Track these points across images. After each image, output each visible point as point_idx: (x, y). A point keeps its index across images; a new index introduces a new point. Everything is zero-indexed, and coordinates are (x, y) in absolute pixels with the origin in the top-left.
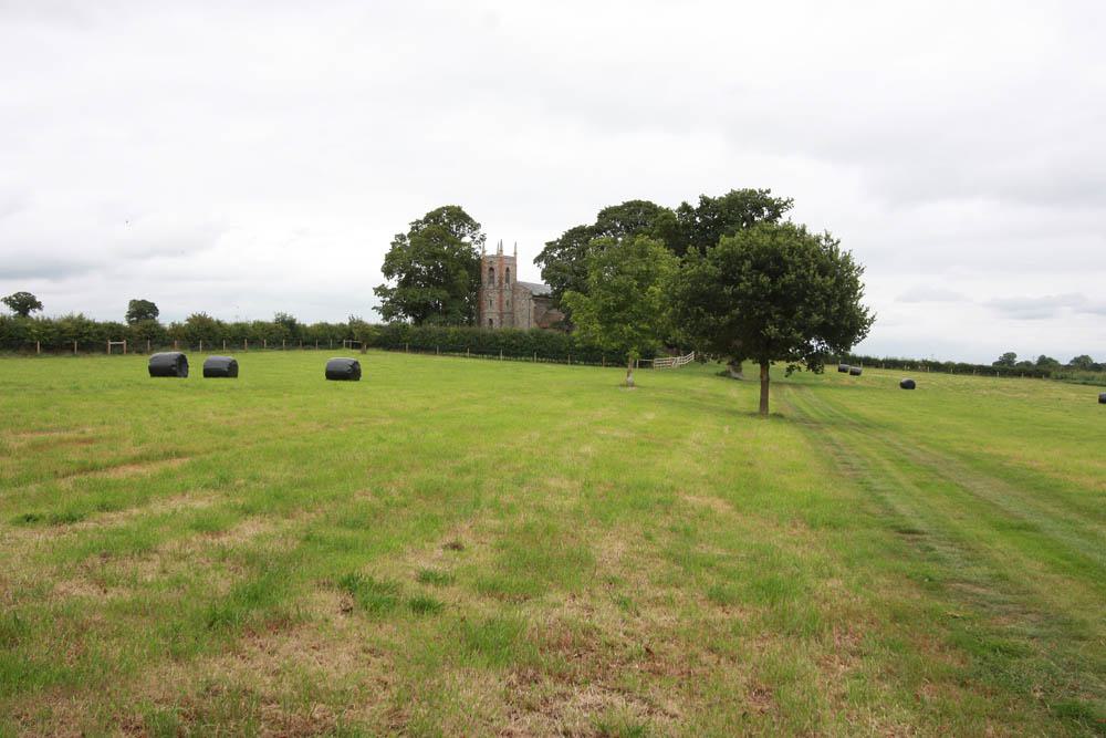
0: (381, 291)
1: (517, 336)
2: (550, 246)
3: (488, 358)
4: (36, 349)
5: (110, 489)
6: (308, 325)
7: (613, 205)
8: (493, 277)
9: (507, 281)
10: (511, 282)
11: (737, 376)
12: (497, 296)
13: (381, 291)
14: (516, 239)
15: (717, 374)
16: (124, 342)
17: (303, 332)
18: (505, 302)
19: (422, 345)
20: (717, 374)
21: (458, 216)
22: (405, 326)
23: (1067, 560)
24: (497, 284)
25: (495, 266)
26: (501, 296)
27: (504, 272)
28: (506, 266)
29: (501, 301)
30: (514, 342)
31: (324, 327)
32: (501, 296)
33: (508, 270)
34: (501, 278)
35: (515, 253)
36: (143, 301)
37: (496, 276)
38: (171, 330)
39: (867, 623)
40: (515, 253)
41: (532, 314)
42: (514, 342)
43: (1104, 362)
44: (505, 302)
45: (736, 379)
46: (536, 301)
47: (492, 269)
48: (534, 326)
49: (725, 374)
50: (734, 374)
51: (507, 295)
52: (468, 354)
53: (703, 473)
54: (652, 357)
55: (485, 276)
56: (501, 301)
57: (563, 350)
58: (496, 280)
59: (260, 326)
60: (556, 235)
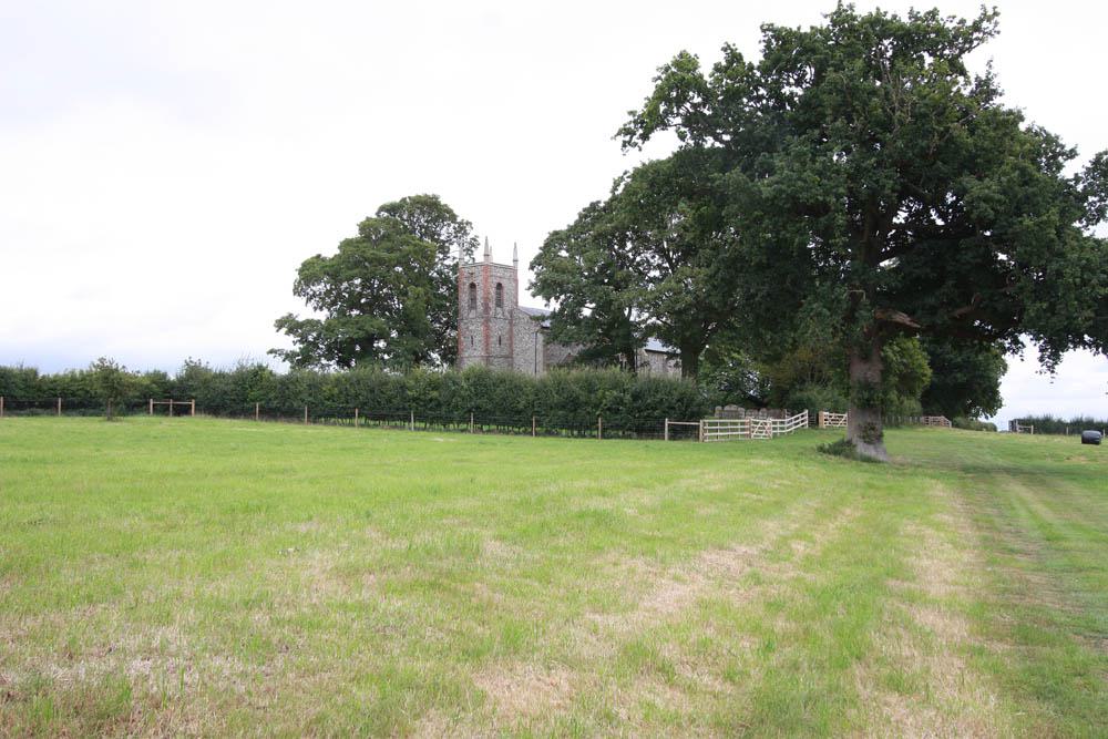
0: (289, 324)
1: (516, 386)
2: (556, 239)
3: (326, 423)
4: (57, 409)
8: (473, 299)
9: (499, 303)
10: (507, 305)
11: (870, 451)
13: (289, 324)
15: (821, 449)
16: (193, 403)
18: (494, 339)
19: (383, 408)
20: (821, 449)
21: (432, 209)
23: (619, 185)
24: (480, 308)
25: (478, 281)
26: (488, 328)
27: (493, 291)
28: (496, 281)
29: (487, 337)
30: (435, 394)
31: (194, 373)
32: (488, 328)
33: (499, 286)
34: (486, 299)
35: (515, 261)
37: (480, 294)
38: (181, 380)
40: (515, 261)
41: (540, 358)
42: (435, 394)
43: (1105, 420)
44: (494, 339)
45: (868, 460)
47: (473, 286)
48: (542, 374)
49: (842, 450)
50: (862, 448)
51: (499, 327)
52: (356, 421)
54: (698, 416)
55: (464, 298)
56: (487, 337)
57: (521, 407)
58: (479, 303)
59: (159, 379)
60: (565, 219)
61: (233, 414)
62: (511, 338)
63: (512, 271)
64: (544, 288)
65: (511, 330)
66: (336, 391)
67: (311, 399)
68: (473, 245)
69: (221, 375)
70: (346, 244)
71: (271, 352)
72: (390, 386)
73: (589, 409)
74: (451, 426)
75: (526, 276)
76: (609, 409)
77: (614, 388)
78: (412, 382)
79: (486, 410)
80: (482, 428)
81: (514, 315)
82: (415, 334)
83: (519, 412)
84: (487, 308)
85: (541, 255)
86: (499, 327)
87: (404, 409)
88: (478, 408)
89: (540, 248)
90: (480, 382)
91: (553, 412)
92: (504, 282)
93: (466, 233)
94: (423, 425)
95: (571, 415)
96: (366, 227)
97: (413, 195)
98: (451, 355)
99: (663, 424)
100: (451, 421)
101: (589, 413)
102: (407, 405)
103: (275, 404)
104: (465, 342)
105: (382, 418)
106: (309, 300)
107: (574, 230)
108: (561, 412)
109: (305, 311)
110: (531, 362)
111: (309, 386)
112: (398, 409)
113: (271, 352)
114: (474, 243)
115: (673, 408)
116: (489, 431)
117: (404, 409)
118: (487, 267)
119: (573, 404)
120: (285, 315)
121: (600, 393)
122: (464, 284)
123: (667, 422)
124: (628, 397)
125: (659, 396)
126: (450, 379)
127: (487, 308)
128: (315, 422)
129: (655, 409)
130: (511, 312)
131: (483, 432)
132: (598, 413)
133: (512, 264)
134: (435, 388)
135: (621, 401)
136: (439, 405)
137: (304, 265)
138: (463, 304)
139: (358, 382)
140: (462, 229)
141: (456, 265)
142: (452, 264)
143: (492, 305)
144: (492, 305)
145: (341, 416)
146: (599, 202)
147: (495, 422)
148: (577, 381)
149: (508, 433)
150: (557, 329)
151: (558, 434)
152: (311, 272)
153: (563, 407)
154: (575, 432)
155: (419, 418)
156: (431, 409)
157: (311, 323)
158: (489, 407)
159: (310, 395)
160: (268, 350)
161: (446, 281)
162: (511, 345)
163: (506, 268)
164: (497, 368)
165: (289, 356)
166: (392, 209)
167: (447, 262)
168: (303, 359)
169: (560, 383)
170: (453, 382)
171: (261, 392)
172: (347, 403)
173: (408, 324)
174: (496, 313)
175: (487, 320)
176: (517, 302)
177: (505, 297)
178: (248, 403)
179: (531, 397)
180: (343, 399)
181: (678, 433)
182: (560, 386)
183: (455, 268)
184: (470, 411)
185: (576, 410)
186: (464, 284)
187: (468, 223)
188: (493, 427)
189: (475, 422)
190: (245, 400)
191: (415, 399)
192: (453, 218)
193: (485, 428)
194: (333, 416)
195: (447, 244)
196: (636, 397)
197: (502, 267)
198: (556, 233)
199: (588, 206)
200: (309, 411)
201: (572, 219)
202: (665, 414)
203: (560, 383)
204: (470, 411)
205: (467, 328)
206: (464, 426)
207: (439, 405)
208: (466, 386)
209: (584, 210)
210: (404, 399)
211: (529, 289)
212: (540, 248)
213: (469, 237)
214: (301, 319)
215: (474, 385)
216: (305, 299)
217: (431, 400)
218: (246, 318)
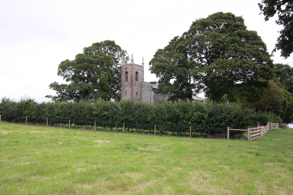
0: (55, 86)
1: (146, 110)
2: (159, 53)
5: (102, 96)
6: (205, 18)
7: (211, 14)
8: (127, 78)
9: (137, 79)
12: (130, 89)
13: (55, 86)
14: (141, 47)
17: (46, 109)
22: (71, 106)
26: (132, 89)
27: (134, 74)
28: (136, 71)
30: (106, 113)
33: (137, 73)
34: (132, 77)
35: (143, 64)
36: (93, 44)
37: (129, 76)
39: (214, 179)
40: (143, 64)
42: (106, 113)
46: (154, 92)
51: (136, 89)
53: (275, 155)
54: (244, 126)
55: (123, 77)
56: (132, 92)
57: (149, 120)
60: (163, 44)
61: (17, 122)
62: (141, 93)
63: (142, 67)
64: (155, 70)
65: (141, 90)
66: (61, 111)
67: (49, 115)
68: (127, 59)
69: (14, 104)
70: (79, 56)
71: (47, 96)
72: (85, 109)
73: (185, 121)
74: (114, 128)
75: (147, 67)
76: (195, 122)
77: (198, 110)
78: (95, 107)
79: (131, 121)
80: (128, 130)
81: (142, 84)
82: (104, 91)
83: (148, 123)
84: (132, 81)
85: (154, 59)
86: (136, 89)
87: (91, 120)
88: (127, 120)
89: (154, 56)
90: (129, 108)
91: (165, 123)
92: (139, 71)
93: (125, 55)
94: (100, 128)
95: (175, 124)
96: (87, 50)
97: (104, 40)
98: (118, 98)
99: (226, 130)
100: (114, 126)
101: (184, 123)
102: (92, 118)
103: (34, 117)
104: (124, 94)
105: (82, 124)
106: (64, 78)
107: (167, 49)
108: (170, 123)
109: (61, 81)
110: (148, 99)
111: (49, 109)
112: (88, 120)
113: (47, 96)
114: (127, 59)
115: (231, 121)
116: (132, 131)
117: (91, 120)
118: (132, 65)
119: (175, 119)
120: (53, 82)
121: (190, 113)
122: (123, 72)
123: (228, 129)
124: (206, 116)
125: (224, 115)
126: (114, 106)
127: (132, 81)
128: (51, 126)
129: (221, 122)
130: (141, 83)
131: (129, 132)
132: (189, 124)
133: (141, 65)
134: (107, 110)
135: (203, 118)
136: (108, 118)
137: (63, 62)
138: (123, 79)
139: (71, 107)
140: (123, 53)
141: (121, 67)
142: (119, 67)
143: (134, 80)
144: (134, 80)
145: (62, 122)
146: (178, 37)
147: (135, 127)
148: (178, 107)
149: (141, 132)
150: (162, 88)
151: (167, 134)
152: (64, 66)
153: (171, 120)
154: (176, 133)
155: (99, 124)
156: (104, 120)
157: (64, 86)
158: (132, 119)
159: (49, 113)
160: (46, 96)
161: (117, 72)
162: (141, 95)
163: (140, 66)
164: (136, 102)
165: (54, 98)
166: (97, 46)
167: (118, 66)
168: (62, 98)
169: (168, 108)
170: (115, 107)
171: (29, 111)
172: (66, 117)
173: (102, 87)
174: (135, 83)
175: (132, 85)
176: (143, 79)
177: (139, 77)
178: (23, 116)
179: (154, 115)
180: (64, 115)
181: (233, 135)
182: (169, 110)
183: (120, 68)
184: (123, 121)
185: (177, 121)
186: (123, 72)
187: (126, 51)
188: (134, 129)
189: (125, 127)
190: (21, 115)
191: (97, 116)
192: (120, 50)
193: (130, 130)
194: (59, 123)
195: (118, 60)
196: (210, 116)
197: (137, 65)
198: (160, 50)
199: (173, 38)
200: (48, 120)
201: (166, 44)
202: (228, 124)
203: (168, 108)
204: (123, 121)
205: (124, 89)
206: (120, 129)
207: (108, 118)
208: (121, 109)
209: (171, 40)
210: (92, 115)
211: (150, 70)
212: (154, 56)
213: (125, 57)
214: (60, 84)
215: (126, 108)
216: (63, 77)
217: (104, 116)
218: (38, 83)
